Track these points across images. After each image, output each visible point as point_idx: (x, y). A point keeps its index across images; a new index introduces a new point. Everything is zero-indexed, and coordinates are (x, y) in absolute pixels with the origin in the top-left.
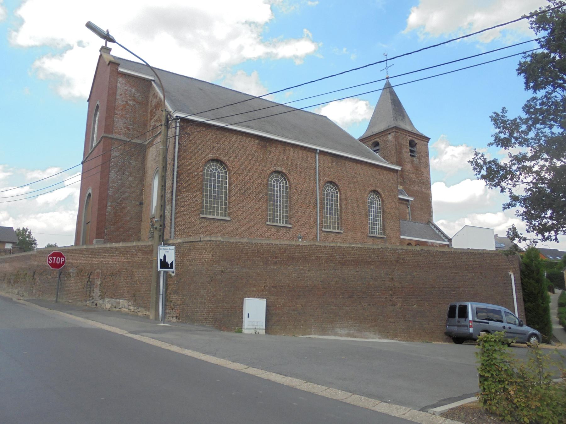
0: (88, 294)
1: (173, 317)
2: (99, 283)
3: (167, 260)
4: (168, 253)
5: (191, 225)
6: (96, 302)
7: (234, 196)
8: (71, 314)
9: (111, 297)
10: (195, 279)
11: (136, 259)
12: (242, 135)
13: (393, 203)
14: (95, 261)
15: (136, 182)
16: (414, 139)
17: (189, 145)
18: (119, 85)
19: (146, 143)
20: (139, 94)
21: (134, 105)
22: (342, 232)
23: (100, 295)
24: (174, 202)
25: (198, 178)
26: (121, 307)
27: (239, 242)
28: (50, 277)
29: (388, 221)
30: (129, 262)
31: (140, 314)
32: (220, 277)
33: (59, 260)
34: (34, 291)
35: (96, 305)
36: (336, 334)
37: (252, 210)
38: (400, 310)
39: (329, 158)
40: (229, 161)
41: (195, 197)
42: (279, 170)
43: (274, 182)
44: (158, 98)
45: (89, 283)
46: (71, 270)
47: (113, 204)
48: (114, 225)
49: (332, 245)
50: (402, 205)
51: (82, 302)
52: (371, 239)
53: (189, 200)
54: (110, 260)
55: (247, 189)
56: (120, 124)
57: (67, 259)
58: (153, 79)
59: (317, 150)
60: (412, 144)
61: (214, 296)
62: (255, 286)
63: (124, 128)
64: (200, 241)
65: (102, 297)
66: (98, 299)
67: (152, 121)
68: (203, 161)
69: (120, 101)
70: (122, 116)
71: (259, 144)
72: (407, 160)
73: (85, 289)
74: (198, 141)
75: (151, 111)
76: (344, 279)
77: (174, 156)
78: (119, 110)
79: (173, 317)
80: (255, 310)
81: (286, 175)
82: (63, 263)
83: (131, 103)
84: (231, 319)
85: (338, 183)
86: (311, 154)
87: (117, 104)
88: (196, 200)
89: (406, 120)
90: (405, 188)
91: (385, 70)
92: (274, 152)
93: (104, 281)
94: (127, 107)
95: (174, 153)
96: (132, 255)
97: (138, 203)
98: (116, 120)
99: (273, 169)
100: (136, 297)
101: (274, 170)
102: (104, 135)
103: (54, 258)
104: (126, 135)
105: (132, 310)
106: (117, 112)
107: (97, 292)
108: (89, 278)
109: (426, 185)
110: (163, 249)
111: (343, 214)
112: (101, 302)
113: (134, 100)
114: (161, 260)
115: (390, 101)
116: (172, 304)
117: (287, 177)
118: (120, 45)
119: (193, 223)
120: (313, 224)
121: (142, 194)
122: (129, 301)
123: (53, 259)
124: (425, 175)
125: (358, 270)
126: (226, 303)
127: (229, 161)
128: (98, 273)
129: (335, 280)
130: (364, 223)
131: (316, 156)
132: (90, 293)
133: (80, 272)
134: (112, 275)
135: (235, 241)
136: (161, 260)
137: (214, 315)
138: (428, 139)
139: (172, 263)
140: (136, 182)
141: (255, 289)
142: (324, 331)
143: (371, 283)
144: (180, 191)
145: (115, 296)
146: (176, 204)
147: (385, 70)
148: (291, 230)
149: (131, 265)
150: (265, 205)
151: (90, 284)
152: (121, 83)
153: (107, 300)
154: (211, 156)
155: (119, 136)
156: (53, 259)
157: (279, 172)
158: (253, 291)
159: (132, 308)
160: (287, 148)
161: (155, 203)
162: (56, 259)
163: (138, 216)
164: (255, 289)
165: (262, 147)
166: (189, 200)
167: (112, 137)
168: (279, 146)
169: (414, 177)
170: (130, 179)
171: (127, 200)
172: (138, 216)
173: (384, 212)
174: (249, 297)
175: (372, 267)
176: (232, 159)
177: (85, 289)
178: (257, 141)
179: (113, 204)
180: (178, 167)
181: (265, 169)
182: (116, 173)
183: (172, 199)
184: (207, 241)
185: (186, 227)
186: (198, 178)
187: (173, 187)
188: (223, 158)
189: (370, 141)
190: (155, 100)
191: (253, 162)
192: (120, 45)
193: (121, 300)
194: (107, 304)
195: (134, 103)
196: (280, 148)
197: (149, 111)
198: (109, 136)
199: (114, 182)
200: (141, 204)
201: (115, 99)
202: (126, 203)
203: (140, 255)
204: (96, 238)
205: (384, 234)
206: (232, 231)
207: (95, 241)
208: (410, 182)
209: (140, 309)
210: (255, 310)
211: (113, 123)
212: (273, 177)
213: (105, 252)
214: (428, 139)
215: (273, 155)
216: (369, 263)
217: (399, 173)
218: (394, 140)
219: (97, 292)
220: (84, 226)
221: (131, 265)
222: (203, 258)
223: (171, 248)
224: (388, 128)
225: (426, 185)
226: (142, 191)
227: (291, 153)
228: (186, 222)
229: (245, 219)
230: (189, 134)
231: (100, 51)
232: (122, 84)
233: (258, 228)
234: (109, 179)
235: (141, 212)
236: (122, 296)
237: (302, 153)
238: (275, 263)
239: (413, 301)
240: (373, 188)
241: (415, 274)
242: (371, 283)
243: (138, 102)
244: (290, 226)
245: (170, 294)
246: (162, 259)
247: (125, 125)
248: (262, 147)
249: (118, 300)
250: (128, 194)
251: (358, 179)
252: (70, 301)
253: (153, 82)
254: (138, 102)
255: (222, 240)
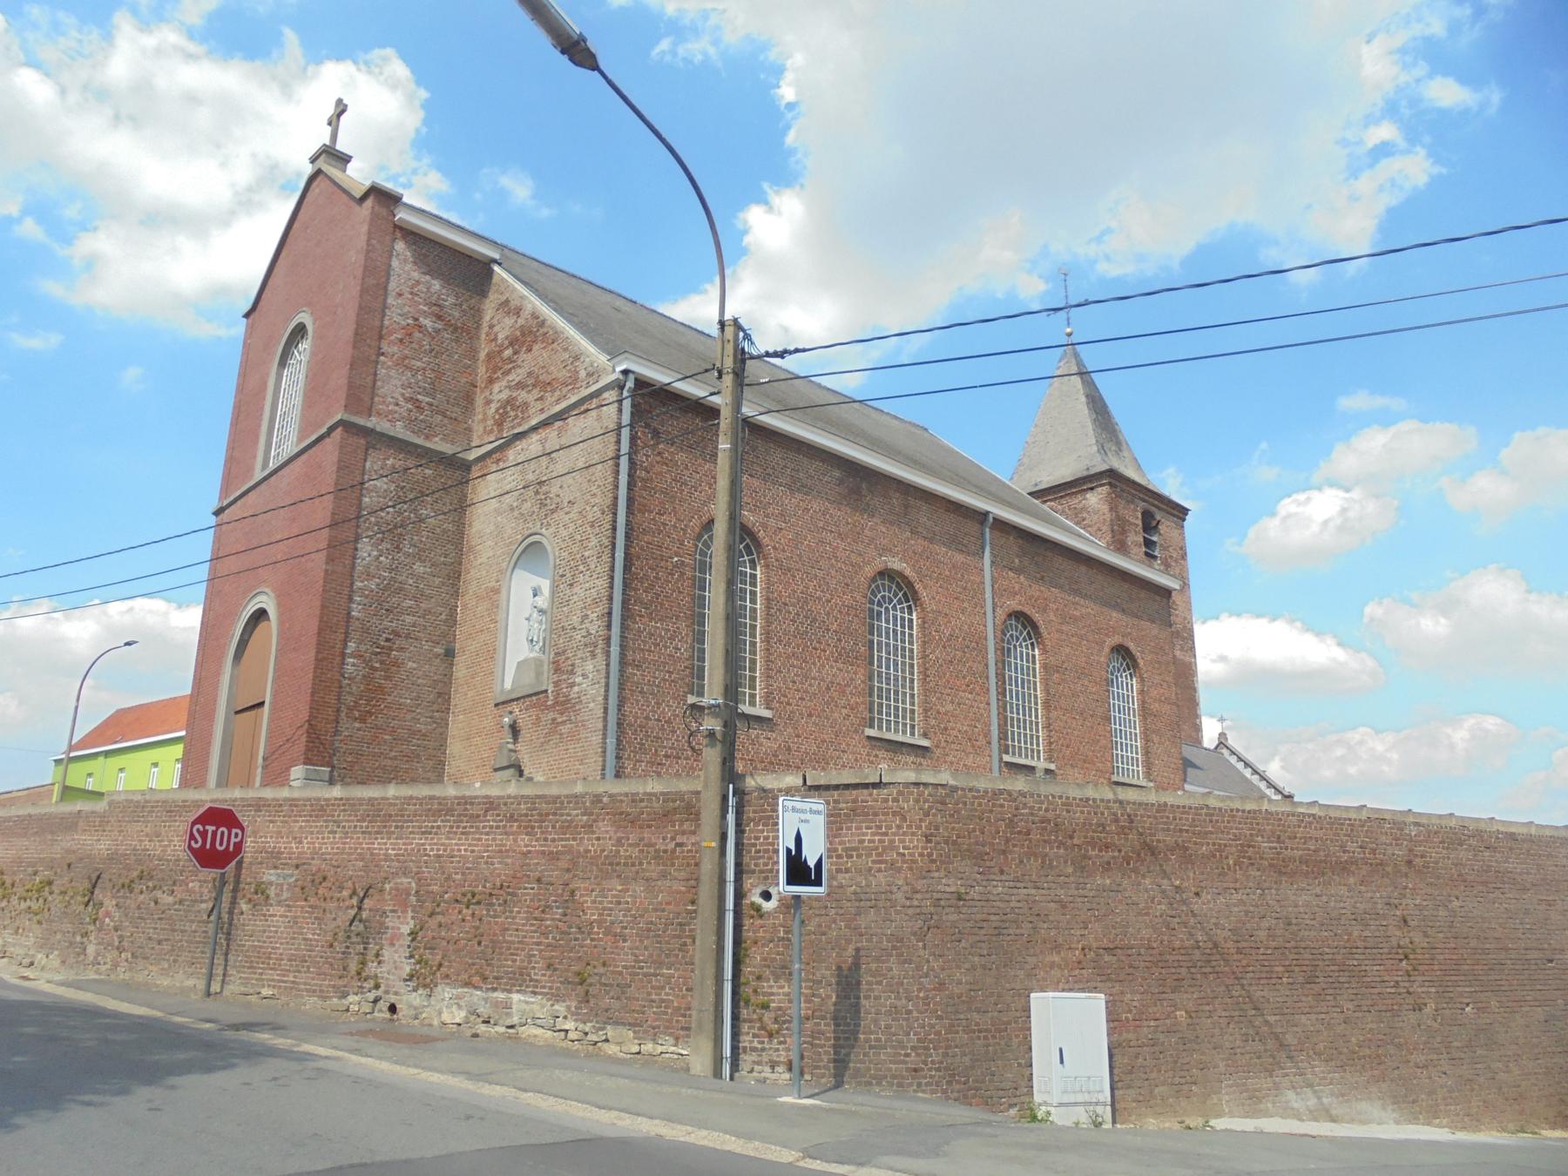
0: (353, 967)
1: (773, 1065)
2: (406, 929)
3: (805, 852)
4: (803, 823)
5: (662, 729)
6: (393, 999)
9: (467, 984)
10: (862, 922)
11: (589, 844)
12: (798, 451)
14: (386, 846)
15: (437, 581)
16: (1153, 509)
17: (657, 468)
18: (395, 263)
19: (472, 456)
20: (451, 300)
21: (438, 331)
23: (411, 977)
24: (615, 649)
25: (682, 574)
26: (515, 1020)
27: (1001, 792)
28: (170, 899)
29: (1156, 739)
30: (553, 857)
31: (611, 1049)
32: (954, 917)
33: (223, 839)
34: (91, 949)
35: (393, 1009)
36: (1289, 1113)
37: (828, 689)
38: (1435, 1025)
40: (764, 526)
41: (672, 638)
43: (880, 605)
44: (525, 314)
45: (358, 927)
46: (270, 876)
47: (363, 648)
48: (363, 721)
49: (1248, 807)
51: (324, 998)
53: (657, 645)
54: (461, 846)
55: (814, 620)
56: (392, 385)
57: (255, 833)
58: (497, 256)
60: (1149, 525)
61: (941, 986)
62: (1056, 948)
63: (408, 400)
64: (878, 785)
65: (422, 979)
66: (401, 986)
67: (496, 387)
69: (397, 312)
70: (402, 363)
71: (841, 482)
73: (338, 947)
75: (489, 356)
77: (616, 498)
78: (391, 343)
79: (773, 1065)
80: (1069, 1035)
81: (910, 585)
82: (239, 847)
83: (427, 322)
84: (987, 1068)
85: (1037, 617)
86: (972, 527)
87: (386, 323)
88: (677, 648)
89: (1126, 454)
93: (433, 923)
94: (417, 335)
95: (617, 487)
96: (568, 827)
97: (439, 650)
98: (382, 372)
100: (583, 986)
101: (881, 567)
102: (346, 417)
103: (210, 828)
104: (410, 422)
105: (571, 1035)
107: (394, 962)
108: (360, 908)
109: (1184, 639)
110: (794, 809)
112: (417, 998)
113: (439, 318)
114: (789, 851)
115: (1083, 399)
116: (768, 1017)
117: (915, 592)
118: (610, 83)
119: (669, 722)
120: (982, 741)
121: (452, 620)
122: (556, 997)
123: (204, 834)
125: (1318, 890)
126: (978, 1011)
127: (764, 526)
128: (401, 896)
129: (1265, 924)
131: (983, 534)
132: (363, 963)
133: (314, 883)
134: (472, 900)
135: (990, 786)
136: (789, 851)
137: (946, 1055)
138: (1185, 511)
139: (819, 864)
140: (437, 581)
141: (1056, 958)
142: (1253, 1104)
143: (1356, 933)
145: (485, 979)
146: (623, 655)
149: (563, 864)
150: (860, 678)
151: (362, 936)
152: (402, 258)
155: (388, 425)
156: (204, 834)
158: (1052, 965)
159: (569, 1025)
160: (912, 501)
162: (214, 834)
163: (440, 694)
164: (1056, 958)
166: (657, 645)
167: (369, 425)
170: (419, 568)
171: (408, 636)
172: (440, 694)
174: (1042, 990)
175: (1352, 880)
177: (338, 947)
178: (837, 474)
179: (363, 648)
180: (628, 536)
182: (375, 545)
183: (608, 640)
184: (907, 785)
186: (682, 574)
187: (611, 599)
190: (509, 321)
191: (830, 537)
192: (610, 83)
193: (516, 997)
194: (448, 1007)
195: (439, 325)
197: (482, 355)
198: (361, 421)
199: (370, 576)
200: (450, 654)
201: (385, 307)
202: (401, 649)
203: (605, 828)
204: (308, 761)
205: (1148, 775)
207: (297, 772)
209: (610, 1031)
210: (1069, 1035)
211: (375, 382)
213: (437, 814)
216: (1344, 868)
218: (1105, 508)
219: (394, 962)
220: (227, 719)
221: (563, 864)
222: (892, 846)
223: (815, 807)
224: (1085, 473)
225: (1184, 639)
226: (453, 609)
228: (647, 718)
229: (810, 715)
232: (405, 261)
234: (353, 566)
235: (448, 677)
236: (520, 980)
238: (1107, 867)
239: (1461, 994)
241: (1456, 903)
242: (1356, 933)
243: (448, 324)
245: (759, 978)
246: (793, 847)
247: (408, 393)
249: (500, 995)
250: (409, 619)
252: (266, 992)
253: (496, 268)
254: (448, 324)
255: (952, 782)
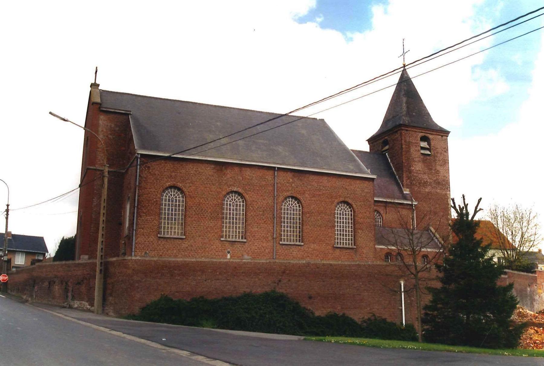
7: (189, 217)
8: (50, 310)
13: (368, 213)
22: (302, 244)
39: (289, 175)
42: (235, 190)
50: (404, 210)
52: (338, 250)
59: (275, 167)
66: (70, 301)
68: (162, 189)
71: (214, 168)
72: (416, 159)
74: (157, 172)
76: (235, 287)
90: (412, 191)
91: (402, 56)
92: (229, 173)
99: (229, 190)
106: (99, 146)
109: (442, 185)
111: (305, 228)
119: (152, 242)
124: (441, 174)
130: (330, 234)
138: (446, 133)
144: (141, 216)
147: (402, 56)
148: (246, 244)
153: (75, 302)
154: (168, 184)
157: (236, 192)
160: (243, 169)
161: (127, 225)
165: (218, 170)
168: (235, 168)
169: (426, 177)
173: (355, 223)
175: (260, 277)
176: (188, 185)
178: (213, 166)
181: (220, 190)
185: (145, 246)
186: (156, 204)
188: (180, 185)
189: (381, 139)
194: (76, 304)
196: (237, 169)
206: (187, 248)
208: (420, 183)
212: (228, 199)
214: (446, 133)
215: (228, 176)
217: (375, 182)
227: (248, 172)
230: (149, 167)
231: (91, 87)
233: (212, 244)
237: (260, 173)
240: (342, 199)
244: (245, 240)
248: (218, 170)
251: (324, 192)
